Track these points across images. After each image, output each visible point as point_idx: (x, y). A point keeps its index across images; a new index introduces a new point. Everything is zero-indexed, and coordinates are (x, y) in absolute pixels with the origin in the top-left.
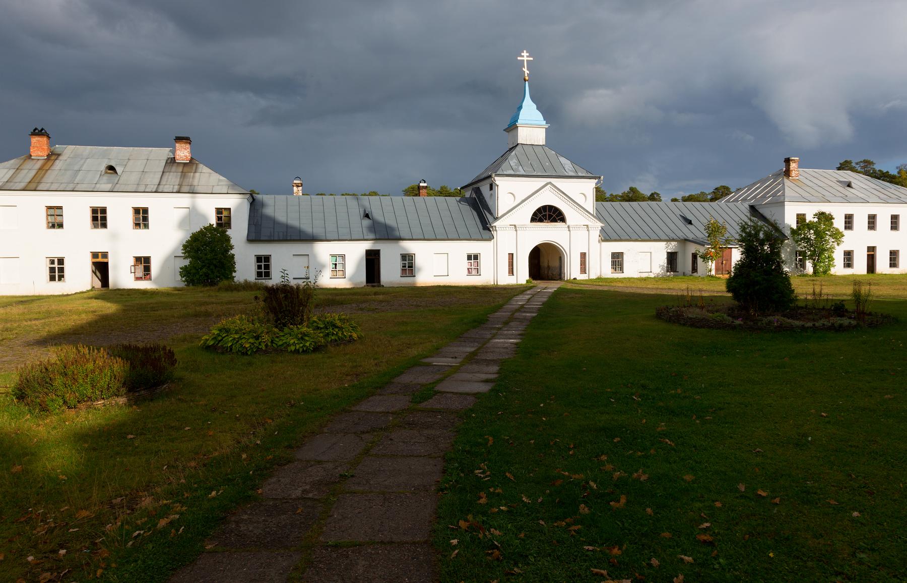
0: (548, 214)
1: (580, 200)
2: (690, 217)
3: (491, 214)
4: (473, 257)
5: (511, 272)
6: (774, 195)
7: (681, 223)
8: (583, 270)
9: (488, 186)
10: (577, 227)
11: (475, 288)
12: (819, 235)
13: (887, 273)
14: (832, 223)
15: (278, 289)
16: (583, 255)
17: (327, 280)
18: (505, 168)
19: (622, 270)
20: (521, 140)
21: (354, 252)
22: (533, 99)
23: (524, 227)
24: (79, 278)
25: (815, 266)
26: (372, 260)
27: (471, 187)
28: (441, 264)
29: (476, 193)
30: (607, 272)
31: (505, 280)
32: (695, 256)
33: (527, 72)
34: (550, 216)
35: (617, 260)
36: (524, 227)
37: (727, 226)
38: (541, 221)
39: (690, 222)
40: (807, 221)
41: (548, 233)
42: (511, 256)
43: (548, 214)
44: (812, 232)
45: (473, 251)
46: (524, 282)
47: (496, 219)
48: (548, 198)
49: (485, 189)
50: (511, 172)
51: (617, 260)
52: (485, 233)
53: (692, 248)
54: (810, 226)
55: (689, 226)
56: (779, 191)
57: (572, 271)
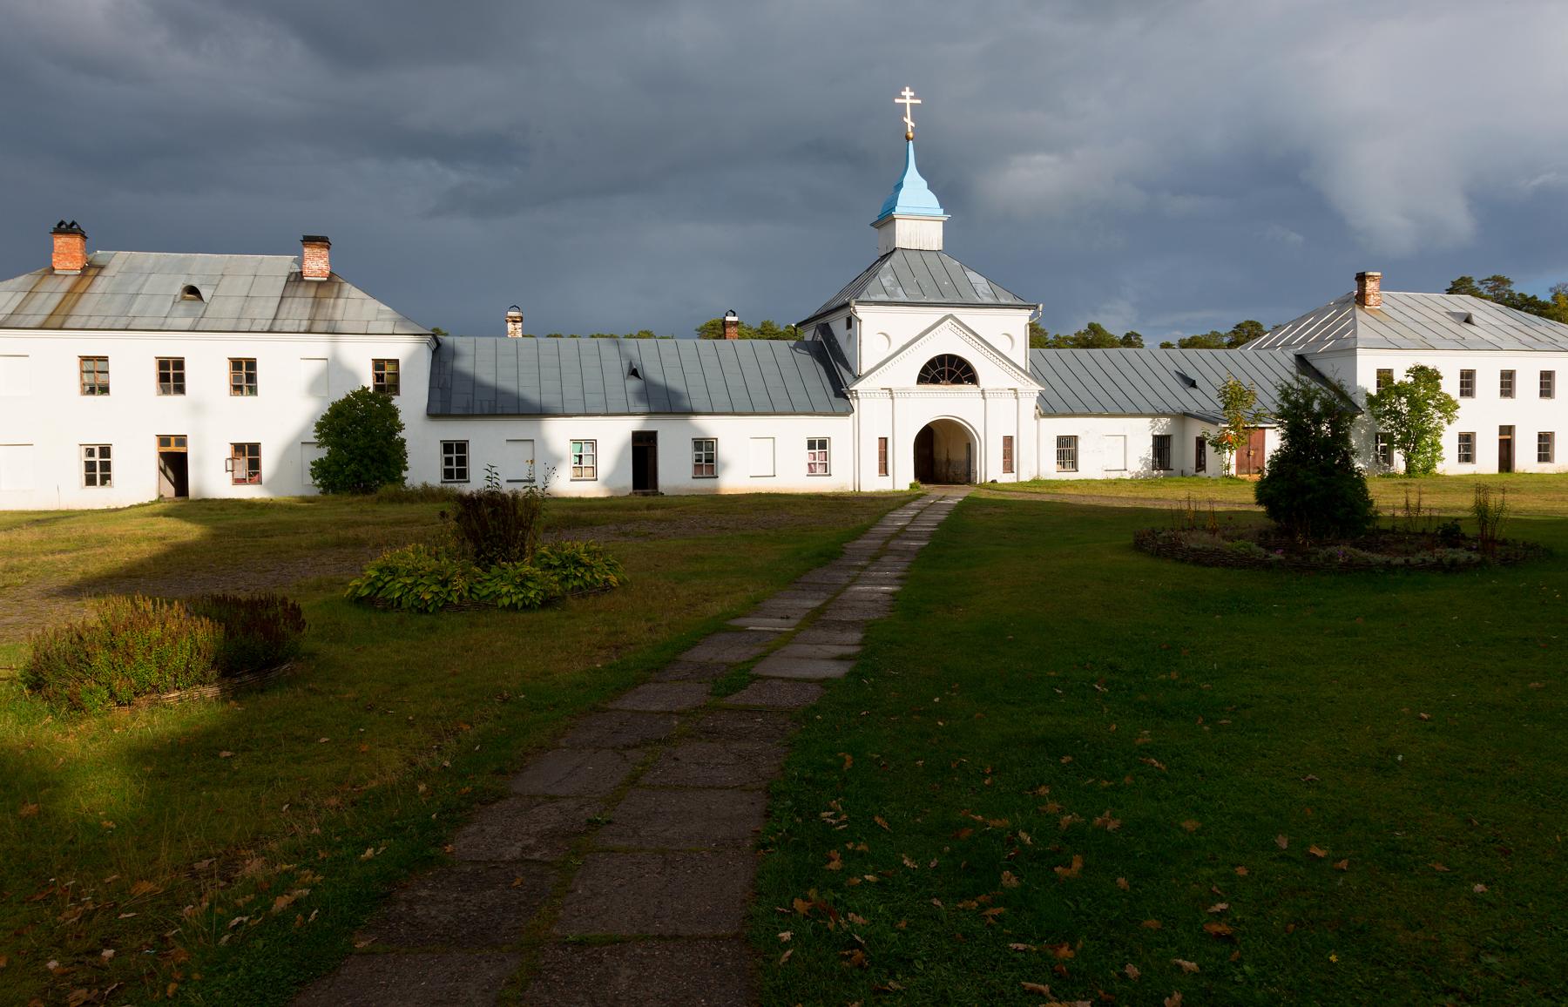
0: (948, 370)
1: (1003, 345)
2: (1193, 375)
3: (849, 369)
4: (818, 444)
5: (884, 469)
6: (1338, 337)
7: (1177, 386)
8: (1008, 467)
9: (844, 321)
10: (998, 392)
11: (821, 498)
12: (1417, 406)
13: (1534, 471)
14: (1438, 386)
15: (480, 499)
16: (1008, 441)
17: (565, 484)
18: (872, 291)
19: (1075, 466)
20: (900, 243)
21: (613, 436)
22: (922, 171)
23: (906, 392)
24: (137, 480)
25: (1408, 460)
26: (644, 449)
27: (814, 324)
28: (762, 455)
29: (823, 334)
30: (1050, 469)
31: (873, 484)
32: (1201, 443)
33: (910, 124)
34: (951, 374)
35: (1067, 449)
36: (906, 392)
37: (1257, 390)
38: (935, 381)
39: (1193, 384)
40: (1396, 382)
41: (947, 402)
42: (884, 442)
43: (948, 370)
44: (1404, 400)
45: (818, 434)
46: (906, 487)
47: (858, 378)
48: (947, 342)
49: (838, 326)
50: (884, 297)
51: (1067, 449)
52: (839, 403)
53: (1197, 429)
54: (1400, 390)
55: (1192, 391)
56: (1346, 330)
57: (990, 468)
